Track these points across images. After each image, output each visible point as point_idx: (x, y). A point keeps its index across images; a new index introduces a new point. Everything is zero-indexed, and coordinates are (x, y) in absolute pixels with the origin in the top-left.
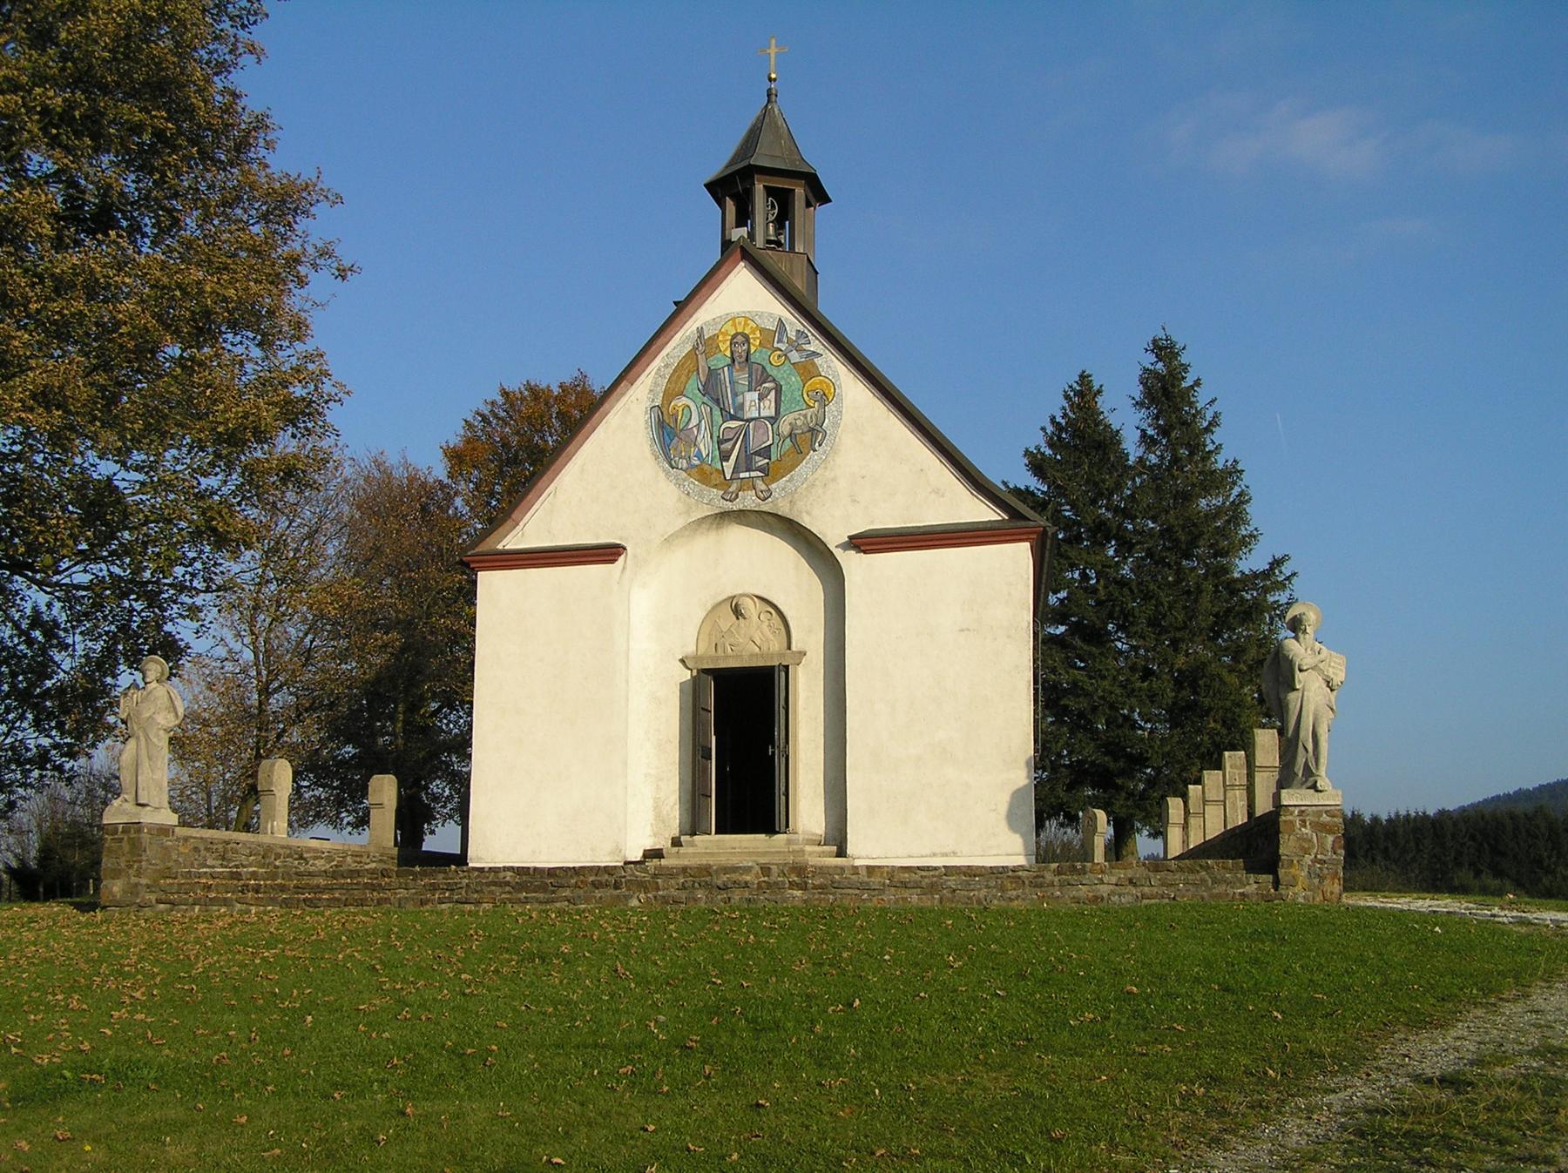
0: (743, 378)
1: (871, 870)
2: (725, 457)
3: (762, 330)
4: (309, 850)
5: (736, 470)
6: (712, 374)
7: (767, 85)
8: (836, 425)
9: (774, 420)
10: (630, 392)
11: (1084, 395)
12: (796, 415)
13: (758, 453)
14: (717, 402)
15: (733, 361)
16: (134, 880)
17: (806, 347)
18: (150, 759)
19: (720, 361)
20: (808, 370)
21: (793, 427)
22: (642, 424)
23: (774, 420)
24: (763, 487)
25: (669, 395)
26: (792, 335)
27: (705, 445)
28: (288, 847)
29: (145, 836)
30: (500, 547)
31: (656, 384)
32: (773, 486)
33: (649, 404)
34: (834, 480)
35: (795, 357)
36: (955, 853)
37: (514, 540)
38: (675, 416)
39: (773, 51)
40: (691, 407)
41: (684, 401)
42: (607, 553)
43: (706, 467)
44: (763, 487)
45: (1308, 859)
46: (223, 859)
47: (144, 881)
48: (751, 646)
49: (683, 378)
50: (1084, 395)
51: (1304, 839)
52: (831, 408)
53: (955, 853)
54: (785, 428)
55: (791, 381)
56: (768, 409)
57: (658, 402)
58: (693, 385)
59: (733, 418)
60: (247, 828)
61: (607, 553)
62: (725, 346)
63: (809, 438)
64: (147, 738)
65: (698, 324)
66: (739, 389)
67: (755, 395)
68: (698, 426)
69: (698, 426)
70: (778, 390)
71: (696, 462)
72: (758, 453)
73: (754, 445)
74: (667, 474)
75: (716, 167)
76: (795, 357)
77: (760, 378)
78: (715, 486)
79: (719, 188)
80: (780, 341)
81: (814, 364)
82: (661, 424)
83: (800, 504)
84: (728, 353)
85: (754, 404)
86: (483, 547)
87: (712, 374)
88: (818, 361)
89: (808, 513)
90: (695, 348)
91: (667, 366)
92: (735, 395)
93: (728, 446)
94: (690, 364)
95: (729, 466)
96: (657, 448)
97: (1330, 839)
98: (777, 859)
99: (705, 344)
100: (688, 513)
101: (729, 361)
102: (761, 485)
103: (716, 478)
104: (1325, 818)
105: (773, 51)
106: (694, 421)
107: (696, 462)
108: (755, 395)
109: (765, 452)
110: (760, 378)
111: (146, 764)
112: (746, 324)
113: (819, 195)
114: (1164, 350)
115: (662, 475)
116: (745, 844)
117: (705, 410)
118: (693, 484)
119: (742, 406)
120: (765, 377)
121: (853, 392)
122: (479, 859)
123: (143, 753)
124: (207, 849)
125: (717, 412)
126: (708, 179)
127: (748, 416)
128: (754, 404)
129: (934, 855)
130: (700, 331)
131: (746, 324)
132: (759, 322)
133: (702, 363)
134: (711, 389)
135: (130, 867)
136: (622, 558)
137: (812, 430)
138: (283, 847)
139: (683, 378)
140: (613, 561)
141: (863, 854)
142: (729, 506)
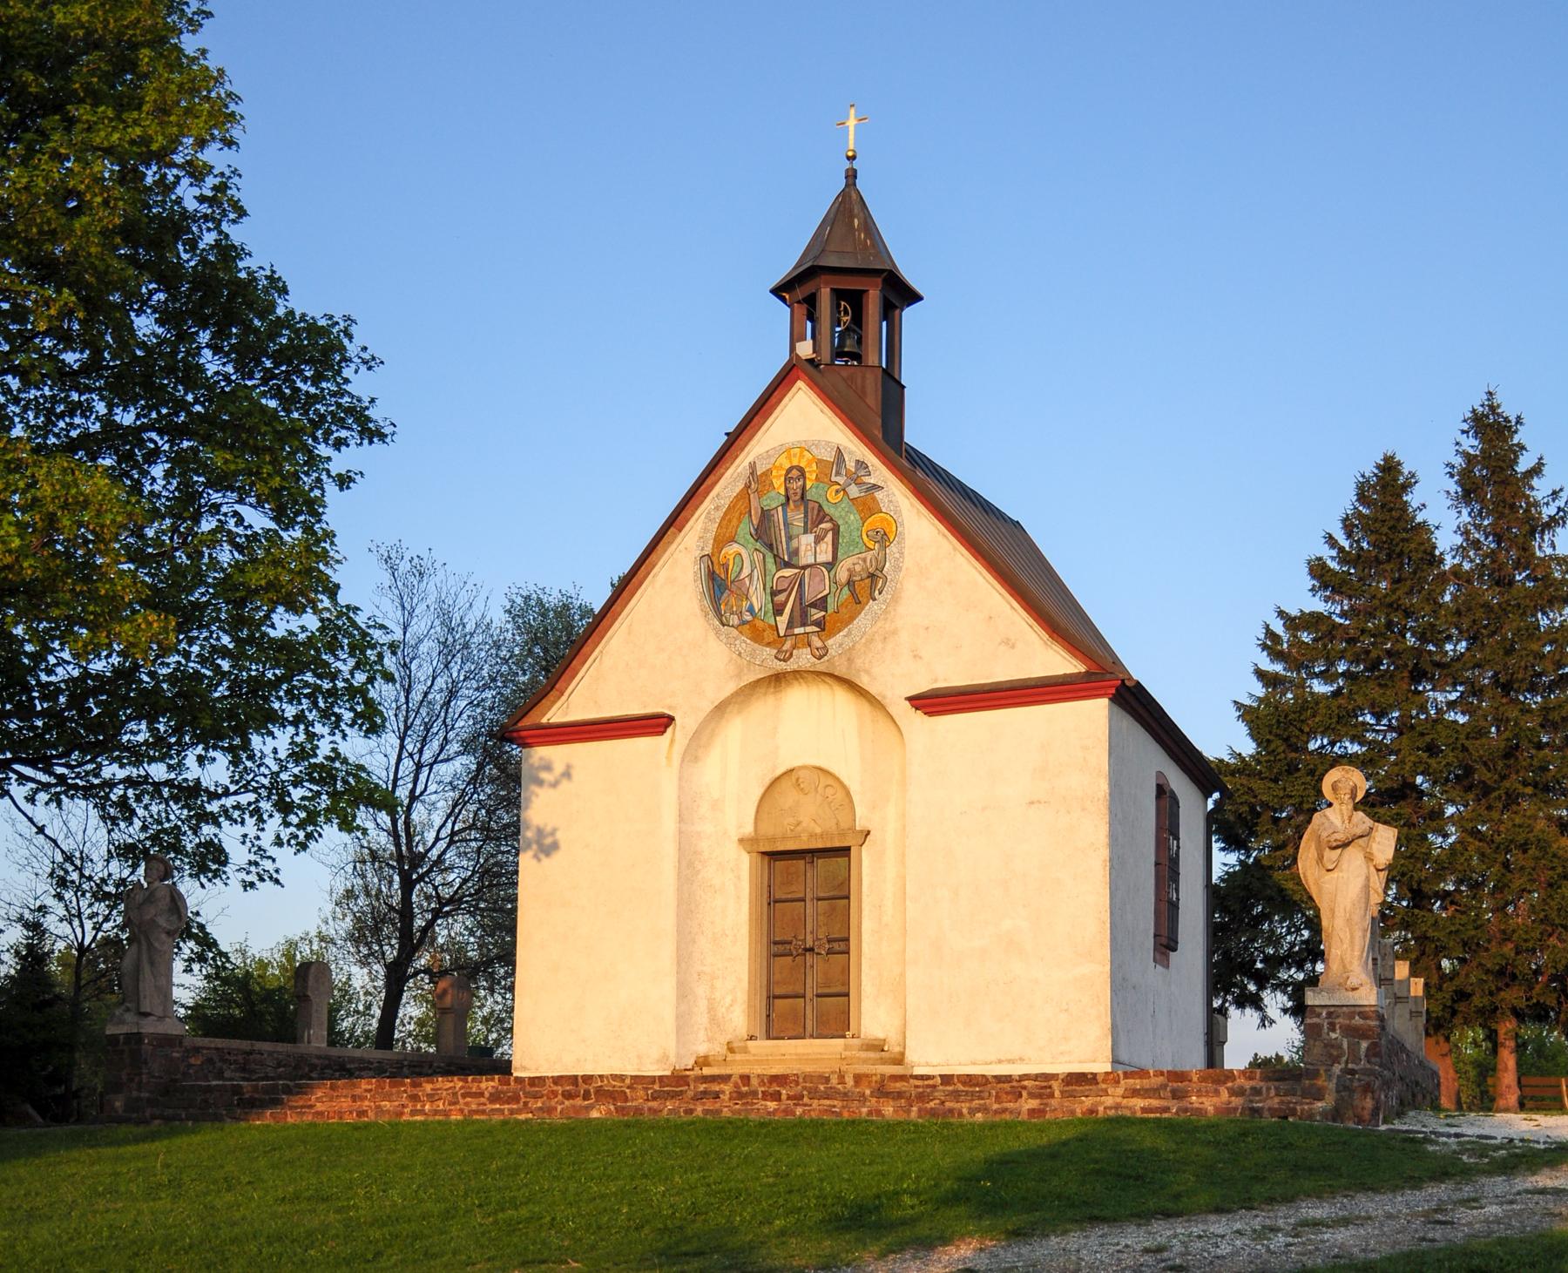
0: (797, 519)
1: (575, 1086)
2: (778, 611)
3: (819, 462)
4: (352, 1060)
5: (790, 625)
6: (766, 515)
7: (847, 165)
8: (898, 569)
9: (830, 566)
10: (679, 539)
11: (1386, 488)
12: (854, 559)
13: (813, 605)
14: (770, 547)
15: (788, 499)
16: (135, 1094)
17: (866, 479)
18: (152, 963)
19: (773, 500)
20: (867, 505)
21: (851, 572)
22: (691, 576)
23: (830, 566)
24: (819, 644)
25: (722, 541)
26: (851, 465)
27: (758, 598)
28: (327, 1057)
29: (146, 1047)
30: (544, 720)
31: (706, 530)
32: (830, 642)
33: (698, 553)
34: (895, 632)
35: (854, 491)
36: (1021, 1059)
37: (558, 713)
38: (725, 566)
39: (852, 123)
40: (744, 556)
41: (735, 548)
42: (657, 724)
43: (759, 624)
44: (819, 644)
45: (1337, 1069)
46: (243, 1070)
47: (145, 1095)
48: (808, 824)
49: (735, 522)
50: (1386, 488)
51: (1330, 1045)
52: (892, 550)
53: (1021, 1059)
54: (842, 574)
55: (850, 520)
56: (825, 554)
57: (708, 551)
58: (745, 529)
59: (788, 565)
60: (279, 1037)
61: (657, 724)
62: (779, 483)
63: (868, 586)
64: (150, 945)
65: (750, 459)
66: (794, 531)
67: (810, 538)
68: (750, 576)
69: (750, 576)
70: (836, 531)
71: (748, 617)
72: (813, 605)
73: (810, 595)
74: (717, 633)
75: (784, 265)
76: (854, 491)
77: (817, 517)
78: (768, 644)
79: (795, 289)
80: (838, 474)
81: (874, 499)
82: (712, 576)
83: (859, 662)
84: (782, 491)
85: (812, 550)
86: (526, 722)
87: (766, 515)
88: (879, 495)
89: (868, 672)
90: (748, 486)
91: (717, 508)
92: (790, 538)
93: (782, 597)
94: (741, 505)
95: (783, 621)
96: (707, 603)
97: (1364, 1045)
98: (758, 1070)
99: (757, 480)
100: (739, 676)
101: (783, 500)
102: (817, 642)
103: (769, 636)
104: (1358, 1021)
105: (852, 123)
106: (746, 572)
107: (748, 617)
108: (810, 538)
109: (821, 604)
110: (817, 517)
111: (147, 968)
112: (802, 456)
113: (900, 294)
114: (1492, 428)
115: (712, 634)
116: (800, 1050)
117: (757, 557)
118: (745, 644)
119: (796, 552)
120: (822, 516)
121: (920, 532)
122: (524, 1068)
123: (145, 957)
124: (223, 1060)
125: (770, 560)
126: (772, 285)
127: (803, 562)
128: (812, 550)
129: (1000, 1062)
130: (753, 466)
131: (802, 456)
132: (815, 452)
133: (754, 503)
134: (764, 533)
135: (132, 1080)
136: (670, 730)
137: (872, 576)
138: (319, 1057)
139: (735, 522)
140: (663, 732)
141: (922, 1061)
142: (781, 666)
